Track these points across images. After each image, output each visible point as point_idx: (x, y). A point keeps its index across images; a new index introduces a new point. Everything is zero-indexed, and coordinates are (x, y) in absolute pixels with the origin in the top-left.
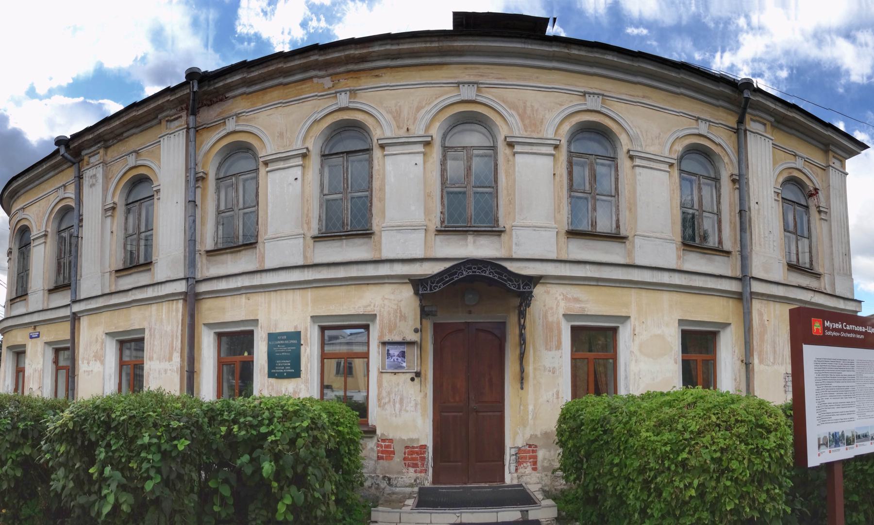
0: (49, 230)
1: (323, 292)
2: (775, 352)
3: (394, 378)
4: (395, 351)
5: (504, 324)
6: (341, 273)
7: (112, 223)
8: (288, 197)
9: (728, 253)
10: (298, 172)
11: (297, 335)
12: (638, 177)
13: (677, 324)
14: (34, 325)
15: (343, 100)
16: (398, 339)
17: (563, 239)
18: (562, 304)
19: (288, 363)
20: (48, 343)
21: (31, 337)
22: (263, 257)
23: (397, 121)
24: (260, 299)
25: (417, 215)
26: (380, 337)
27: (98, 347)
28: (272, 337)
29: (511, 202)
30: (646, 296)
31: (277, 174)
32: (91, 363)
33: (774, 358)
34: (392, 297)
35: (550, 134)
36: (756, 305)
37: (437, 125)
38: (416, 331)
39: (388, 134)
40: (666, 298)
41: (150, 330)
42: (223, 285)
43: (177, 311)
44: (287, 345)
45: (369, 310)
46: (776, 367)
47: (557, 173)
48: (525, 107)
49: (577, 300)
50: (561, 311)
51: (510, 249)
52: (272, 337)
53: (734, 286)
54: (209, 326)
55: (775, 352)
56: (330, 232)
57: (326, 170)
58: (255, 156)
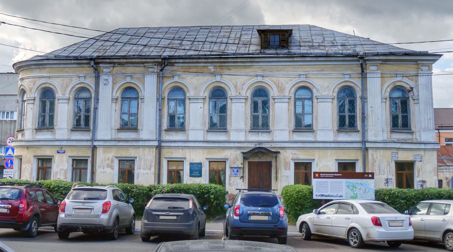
0: (71, 97)
1: (211, 150)
2: (380, 170)
3: (235, 178)
4: (235, 170)
5: (271, 162)
6: (217, 145)
7: (116, 105)
8: (197, 113)
9: (358, 131)
10: (201, 105)
11: (200, 164)
12: (319, 107)
13: (334, 161)
14: (61, 147)
15: (218, 78)
16: (236, 166)
17: (291, 133)
18: (291, 155)
19: (198, 172)
20: (70, 157)
21: (58, 152)
22: (188, 136)
23: (236, 89)
24: (187, 151)
25: (242, 125)
26: (230, 165)
27: (110, 162)
28: (191, 164)
29: (274, 121)
30: (322, 152)
31: (194, 104)
32: (105, 169)
33: (379, 172)
34: (234, 153)
35: (287, 95)
36: (370, 152)
37: (249, 91)
38: (242, 164)
39: (233, 95)
40: (329, 152)
41: (139, 158)
42: (173, 144)
43: (153, 152)
44: (197, 167)
45: (226, 157)
46: (380, 176)
47: (290, 109)
48: (279, 83)
49: (295, 154)
50: (291, 158)
51: (273, 137)
52: (191, 164)
53: (359, 145)
54: (166, 158)
55: (380, 170)
56: (213, 127)
57: (211, 103)
58: (184, 94)
